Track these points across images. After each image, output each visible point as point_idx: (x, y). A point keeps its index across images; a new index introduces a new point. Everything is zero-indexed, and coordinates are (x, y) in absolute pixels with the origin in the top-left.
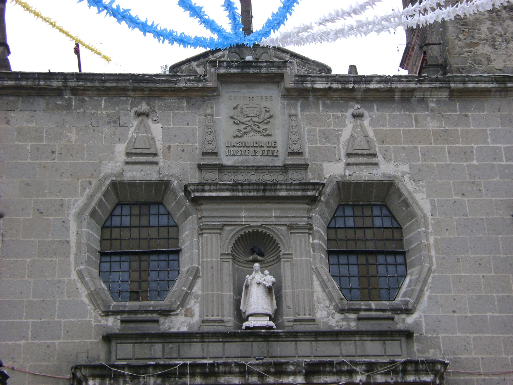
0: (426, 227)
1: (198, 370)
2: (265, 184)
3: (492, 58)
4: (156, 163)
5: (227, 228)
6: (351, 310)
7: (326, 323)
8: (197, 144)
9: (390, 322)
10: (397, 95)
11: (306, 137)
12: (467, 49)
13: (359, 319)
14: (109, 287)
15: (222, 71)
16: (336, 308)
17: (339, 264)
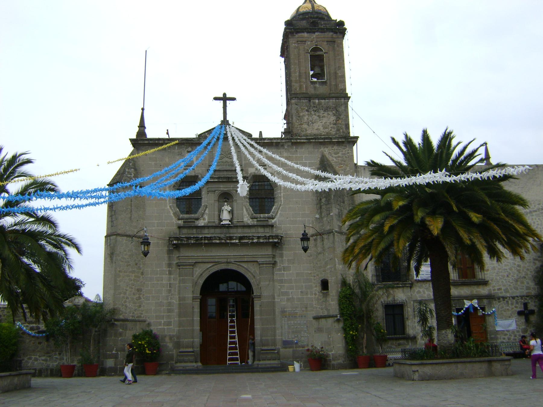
0: (281, 190)
1: (206, 239)
2: (229, 177)
3: (307, 129)
5: (216, 191)
7: (247, 222)
8: (207, 162)
9: (267, 222)
11: (243, 159)
12: (299, 126)
13: (257, 221)
14: (179, 210)
17: (253, 202)
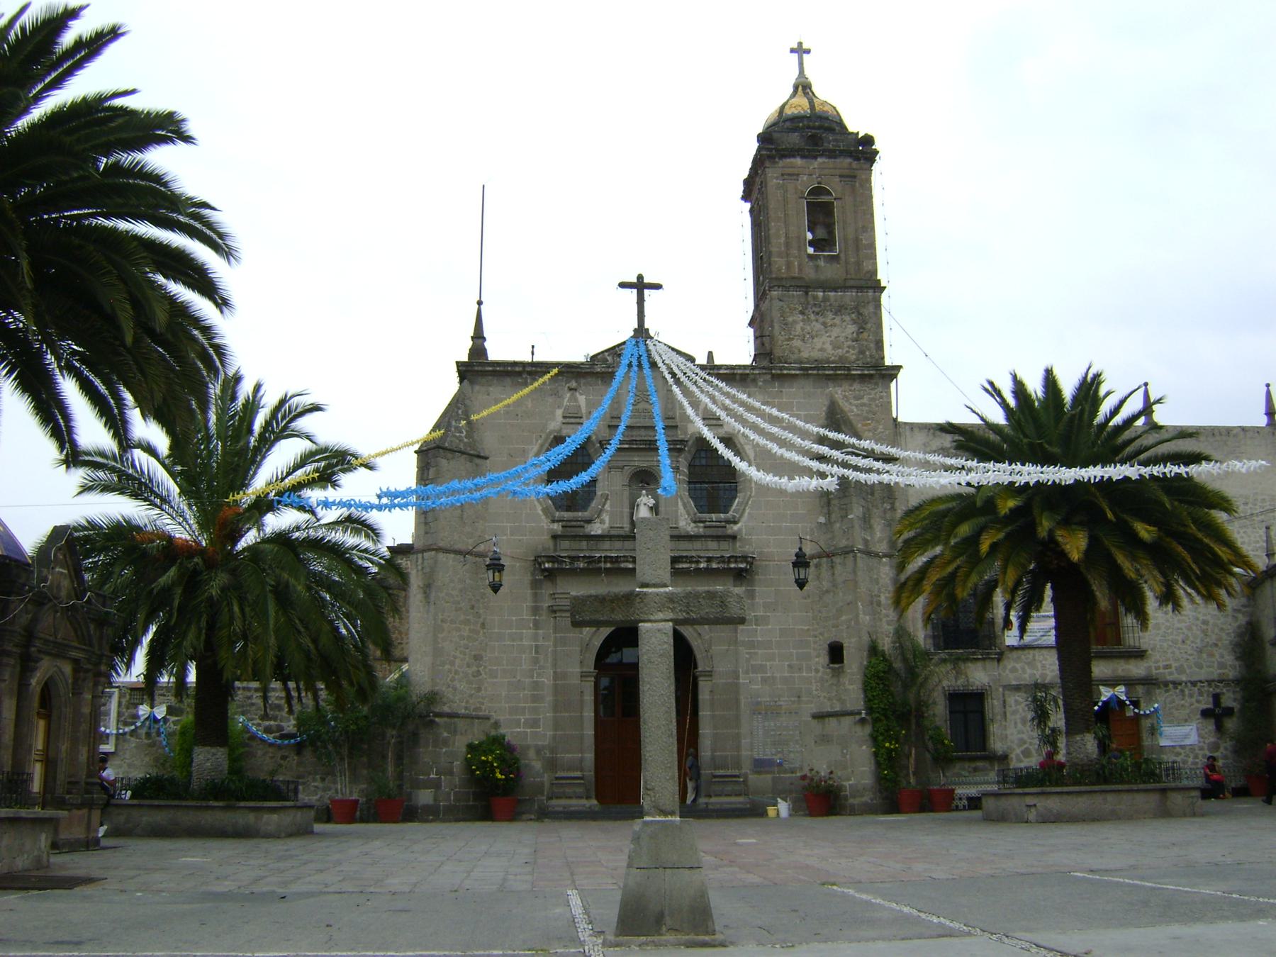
6: (701, 522)
10: (738, 377)
12: (786, 343)
16: (691, 520)
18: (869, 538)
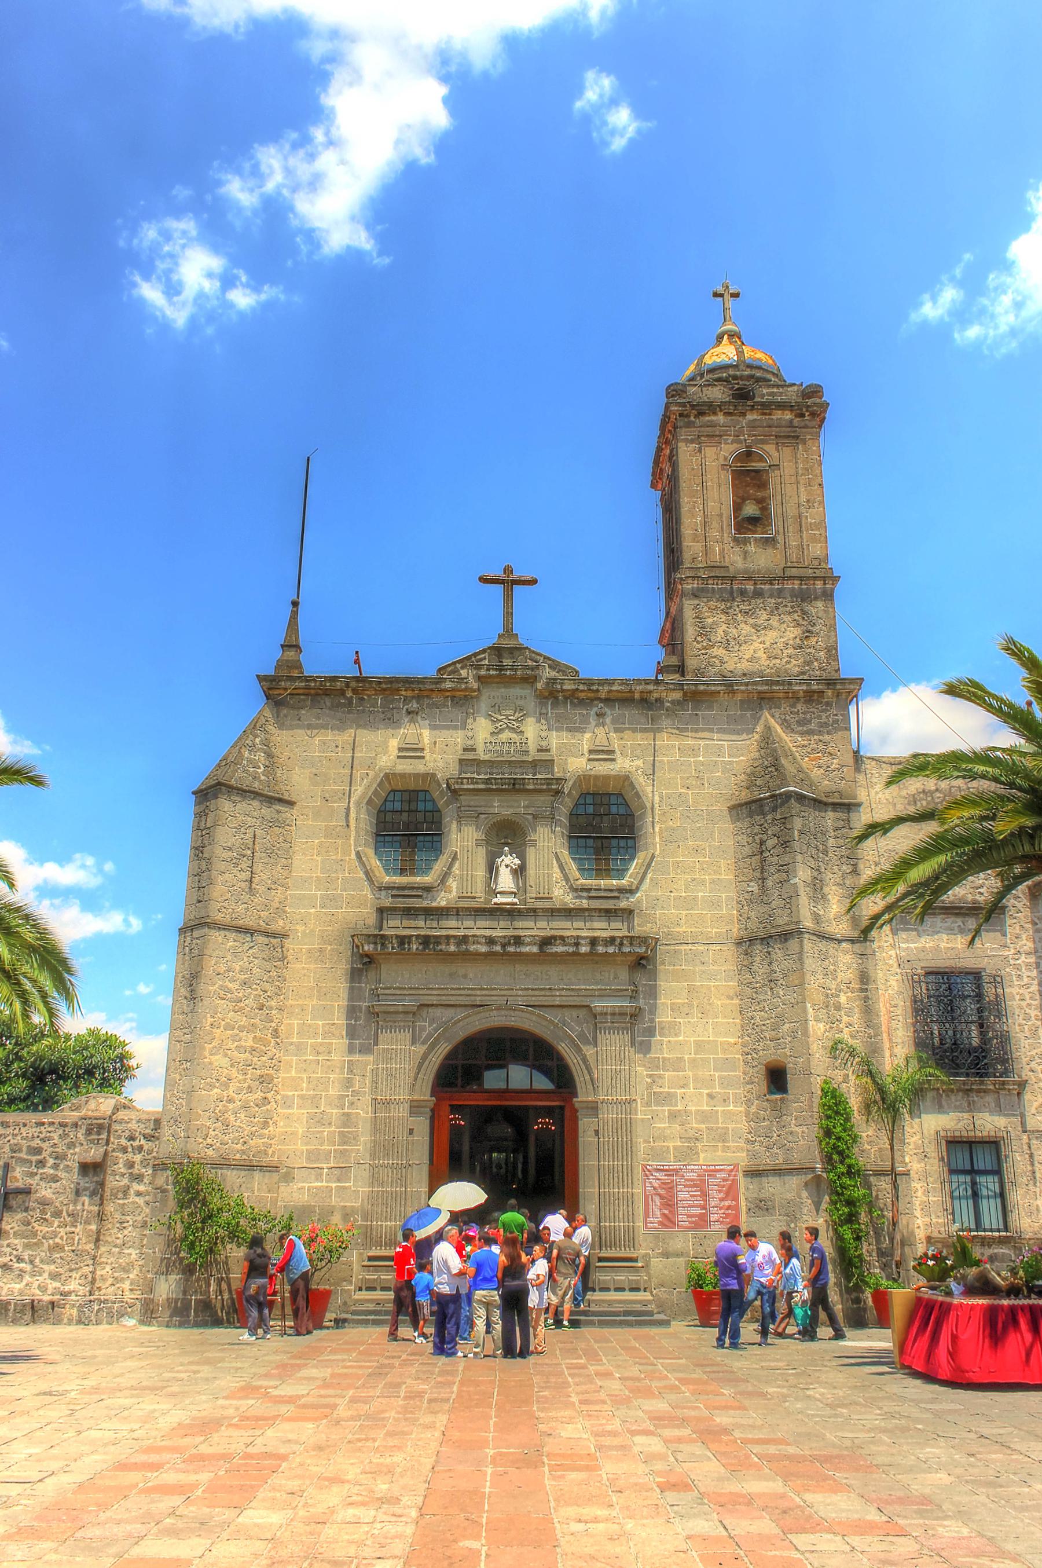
4: (423, 757)
15: (483, 672)
18: (821, 913)
